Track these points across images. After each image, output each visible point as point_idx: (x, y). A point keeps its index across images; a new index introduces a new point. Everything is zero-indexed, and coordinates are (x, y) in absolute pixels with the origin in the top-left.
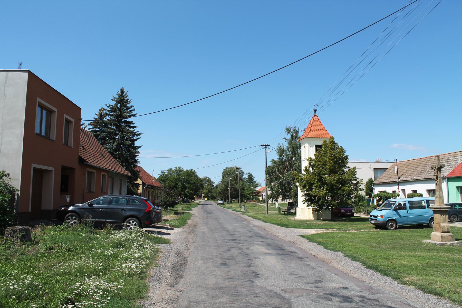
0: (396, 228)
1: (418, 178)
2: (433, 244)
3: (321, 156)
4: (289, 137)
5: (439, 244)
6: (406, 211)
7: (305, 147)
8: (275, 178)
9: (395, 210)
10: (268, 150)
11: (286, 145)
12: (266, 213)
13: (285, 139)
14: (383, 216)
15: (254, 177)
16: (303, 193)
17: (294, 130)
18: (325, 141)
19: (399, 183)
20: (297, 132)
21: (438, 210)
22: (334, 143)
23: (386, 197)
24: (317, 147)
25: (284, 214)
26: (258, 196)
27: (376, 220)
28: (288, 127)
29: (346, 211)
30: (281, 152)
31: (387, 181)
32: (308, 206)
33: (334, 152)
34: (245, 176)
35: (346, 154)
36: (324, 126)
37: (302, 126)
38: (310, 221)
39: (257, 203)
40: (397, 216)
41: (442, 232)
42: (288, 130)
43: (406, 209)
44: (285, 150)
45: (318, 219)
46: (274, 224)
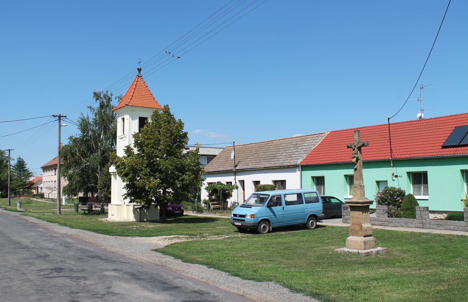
0: (269, 232)
1: (263, 166)
2: (354, 254)
3: (152, 132)
4: (97, 105)
5: (364, 253)
6: (281, 207)
7: (123, 119)
8: (75, 162)
9: (269, 206)
10: (63, 123)
11: (91, 117)
12: (58, 213)
13: (90, 107)
14: (253, 215)
15: (26, 163)
16: (125, 184)
17: (105, 96)
18: (156, 112)
19: (235, 172)
20: (109, 99)
21: (360, 205)
22: (169, 114)
23: (222, 189)
24: (142, 121)
25: (85, 214)
26: (32, 189)
27: (244, 220)
28: (97, 92)
29: (174, 208)
30: (84, 125)
31: (220, 169)
32: (130, 202)
33: (170, 127)
34: (13, 163)
35: (184, 131)
36: (152, 92)
37: (118, 90)
38: (131, 223)
39: (32, 199)
40: (272, 214)
41: (365, 237)
42: (97, 96)
43: (281, 205)
44: (89, 124)
45: (141, 221)
46: (89, 230)
